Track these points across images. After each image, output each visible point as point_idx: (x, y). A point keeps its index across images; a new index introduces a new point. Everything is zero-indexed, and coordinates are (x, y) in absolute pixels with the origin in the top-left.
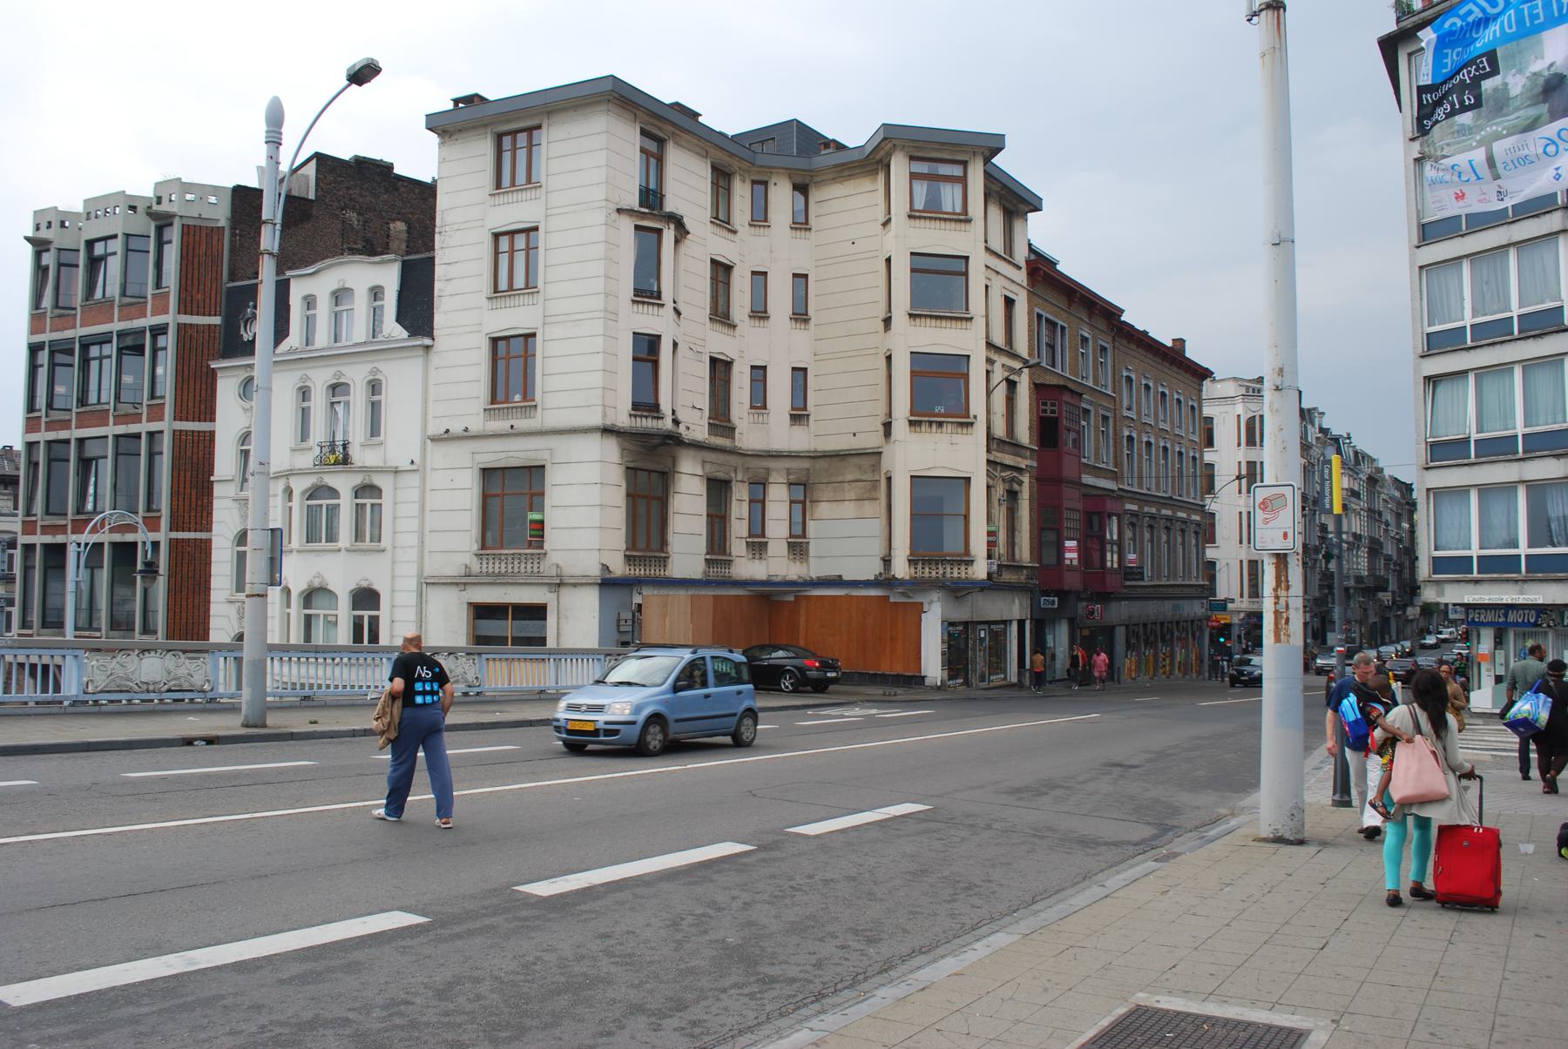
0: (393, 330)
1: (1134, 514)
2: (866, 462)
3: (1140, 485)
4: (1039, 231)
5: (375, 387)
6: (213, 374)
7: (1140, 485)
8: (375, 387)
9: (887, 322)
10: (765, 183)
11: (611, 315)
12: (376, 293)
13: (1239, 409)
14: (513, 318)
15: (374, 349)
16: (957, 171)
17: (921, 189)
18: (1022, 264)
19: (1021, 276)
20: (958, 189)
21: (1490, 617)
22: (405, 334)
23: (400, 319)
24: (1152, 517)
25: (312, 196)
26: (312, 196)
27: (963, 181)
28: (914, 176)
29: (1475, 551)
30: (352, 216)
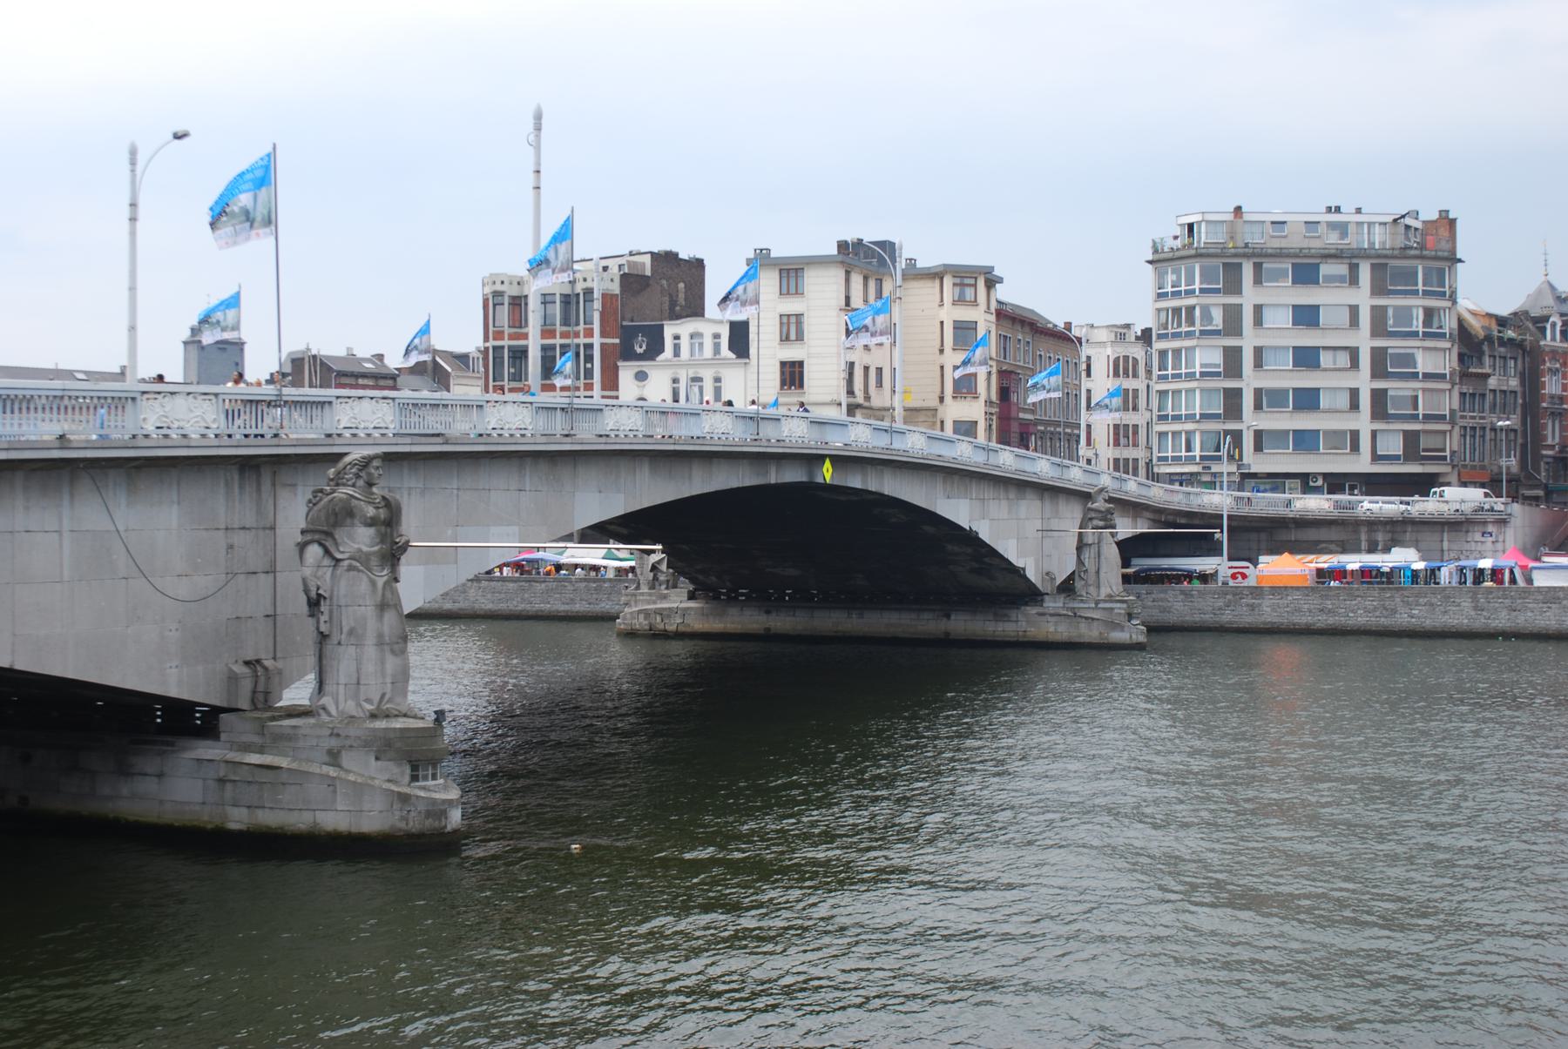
0: (725, 351)
1: (1043, 432)
2: (929, 413)
3: (1045, 415)
4: (1002, 293)
5: (718, 380)
6: (617, 368)
7: (1045, 415)
8: (718, 380)
9: (942, 351)
10: (881, 280)
11: (839, 354)
12: (717, 336)
13: (1109, 351)
14: (792, 353)
15: (725, 363)
16: (972, 281)
17: (957, 290)
18: (993, 311)
19: (993, 318)
20: (973, 289)
21: (1177, 477)
22: (734, 356)
23: (731, 348)
24: (1052, 433)
25: (648, 273)
26: (648, 273)
27: (975, 286)
28: (954, 285)
29: (1170, 454)
30: (664, 282)
